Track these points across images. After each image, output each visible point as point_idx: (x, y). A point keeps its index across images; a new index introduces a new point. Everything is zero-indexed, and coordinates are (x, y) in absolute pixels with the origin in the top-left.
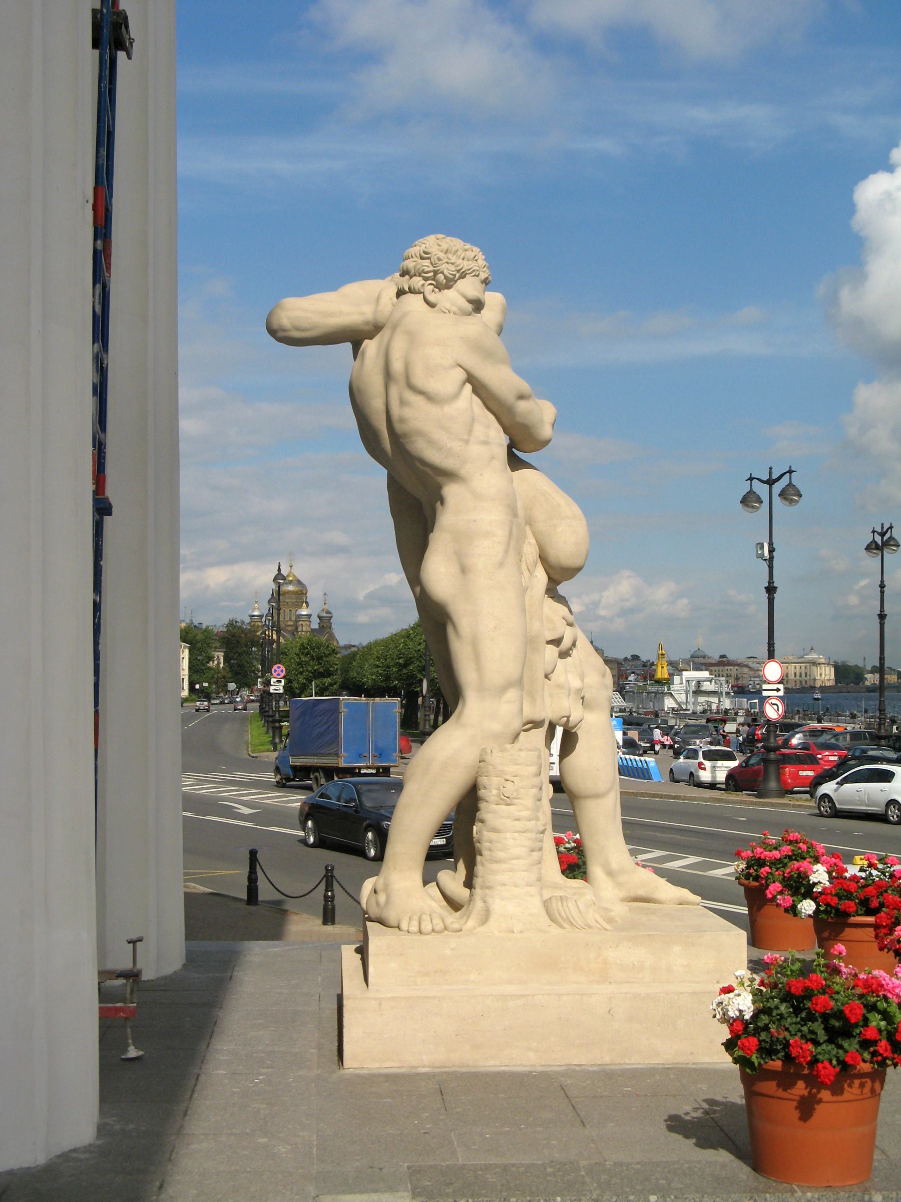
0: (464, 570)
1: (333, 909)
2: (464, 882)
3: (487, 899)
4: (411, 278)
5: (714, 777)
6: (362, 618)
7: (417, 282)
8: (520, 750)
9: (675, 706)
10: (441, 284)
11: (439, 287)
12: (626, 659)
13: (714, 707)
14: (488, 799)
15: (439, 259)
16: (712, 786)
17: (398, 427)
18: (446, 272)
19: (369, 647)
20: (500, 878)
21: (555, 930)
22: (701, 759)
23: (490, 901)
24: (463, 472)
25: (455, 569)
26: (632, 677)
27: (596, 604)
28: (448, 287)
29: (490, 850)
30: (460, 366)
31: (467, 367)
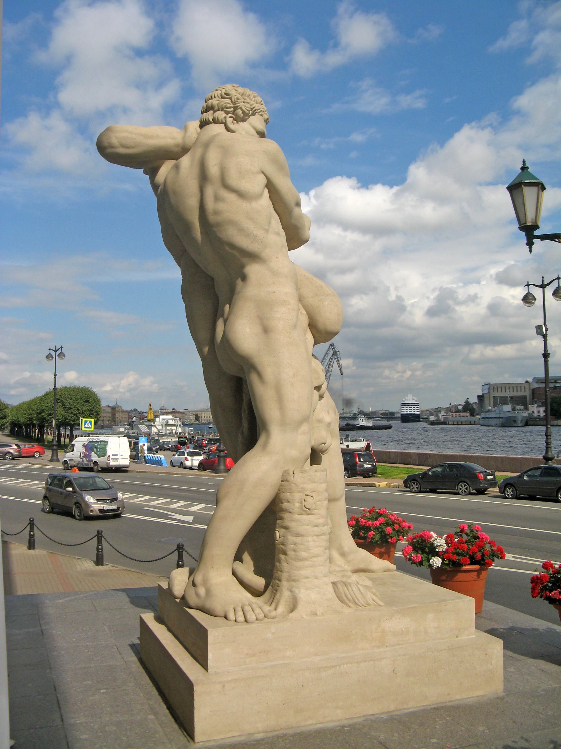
0: (266, 330)
1: (34, 541)
2: (254, 571)
3: (294, 589)
4: (214, 112)
5: (192, 464)
6: (13, 392)
7: (221, 115)
8: (316, 471)
9: (157, 431)
10: (239, 117)
11: (237, 119)
12: (131, 410)
13: (174, 431)
14: (291, 511)
15: (238, 99)
16: (190, 468)
17: (212, 218)
18: (244, 108)
19: (20, 405)
20: (303, 572)
21: (347, 611)
22: (186, 456)
23: (296, 591)
24: (264, 255)
25: (257, 329)
26: (134, 419)
27: (118, 386)
28: (244, 120)
29: (295, 551)
30: (263, 173)
31: (268, 174)
